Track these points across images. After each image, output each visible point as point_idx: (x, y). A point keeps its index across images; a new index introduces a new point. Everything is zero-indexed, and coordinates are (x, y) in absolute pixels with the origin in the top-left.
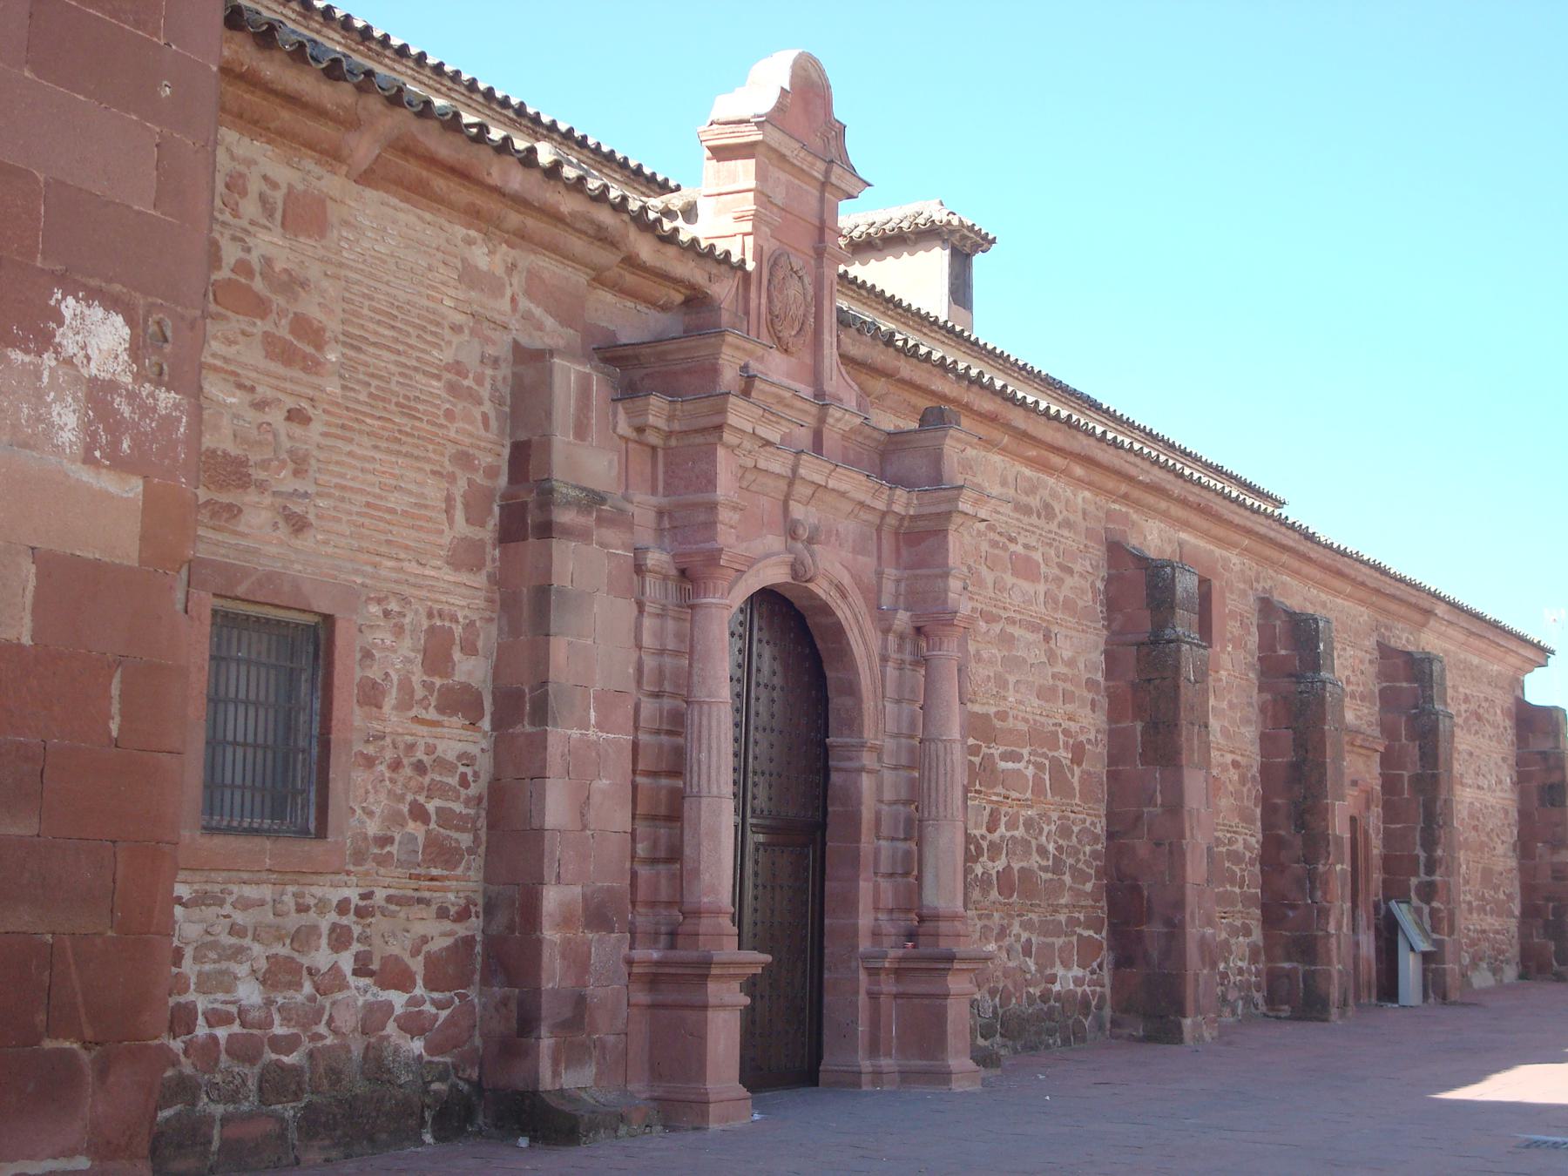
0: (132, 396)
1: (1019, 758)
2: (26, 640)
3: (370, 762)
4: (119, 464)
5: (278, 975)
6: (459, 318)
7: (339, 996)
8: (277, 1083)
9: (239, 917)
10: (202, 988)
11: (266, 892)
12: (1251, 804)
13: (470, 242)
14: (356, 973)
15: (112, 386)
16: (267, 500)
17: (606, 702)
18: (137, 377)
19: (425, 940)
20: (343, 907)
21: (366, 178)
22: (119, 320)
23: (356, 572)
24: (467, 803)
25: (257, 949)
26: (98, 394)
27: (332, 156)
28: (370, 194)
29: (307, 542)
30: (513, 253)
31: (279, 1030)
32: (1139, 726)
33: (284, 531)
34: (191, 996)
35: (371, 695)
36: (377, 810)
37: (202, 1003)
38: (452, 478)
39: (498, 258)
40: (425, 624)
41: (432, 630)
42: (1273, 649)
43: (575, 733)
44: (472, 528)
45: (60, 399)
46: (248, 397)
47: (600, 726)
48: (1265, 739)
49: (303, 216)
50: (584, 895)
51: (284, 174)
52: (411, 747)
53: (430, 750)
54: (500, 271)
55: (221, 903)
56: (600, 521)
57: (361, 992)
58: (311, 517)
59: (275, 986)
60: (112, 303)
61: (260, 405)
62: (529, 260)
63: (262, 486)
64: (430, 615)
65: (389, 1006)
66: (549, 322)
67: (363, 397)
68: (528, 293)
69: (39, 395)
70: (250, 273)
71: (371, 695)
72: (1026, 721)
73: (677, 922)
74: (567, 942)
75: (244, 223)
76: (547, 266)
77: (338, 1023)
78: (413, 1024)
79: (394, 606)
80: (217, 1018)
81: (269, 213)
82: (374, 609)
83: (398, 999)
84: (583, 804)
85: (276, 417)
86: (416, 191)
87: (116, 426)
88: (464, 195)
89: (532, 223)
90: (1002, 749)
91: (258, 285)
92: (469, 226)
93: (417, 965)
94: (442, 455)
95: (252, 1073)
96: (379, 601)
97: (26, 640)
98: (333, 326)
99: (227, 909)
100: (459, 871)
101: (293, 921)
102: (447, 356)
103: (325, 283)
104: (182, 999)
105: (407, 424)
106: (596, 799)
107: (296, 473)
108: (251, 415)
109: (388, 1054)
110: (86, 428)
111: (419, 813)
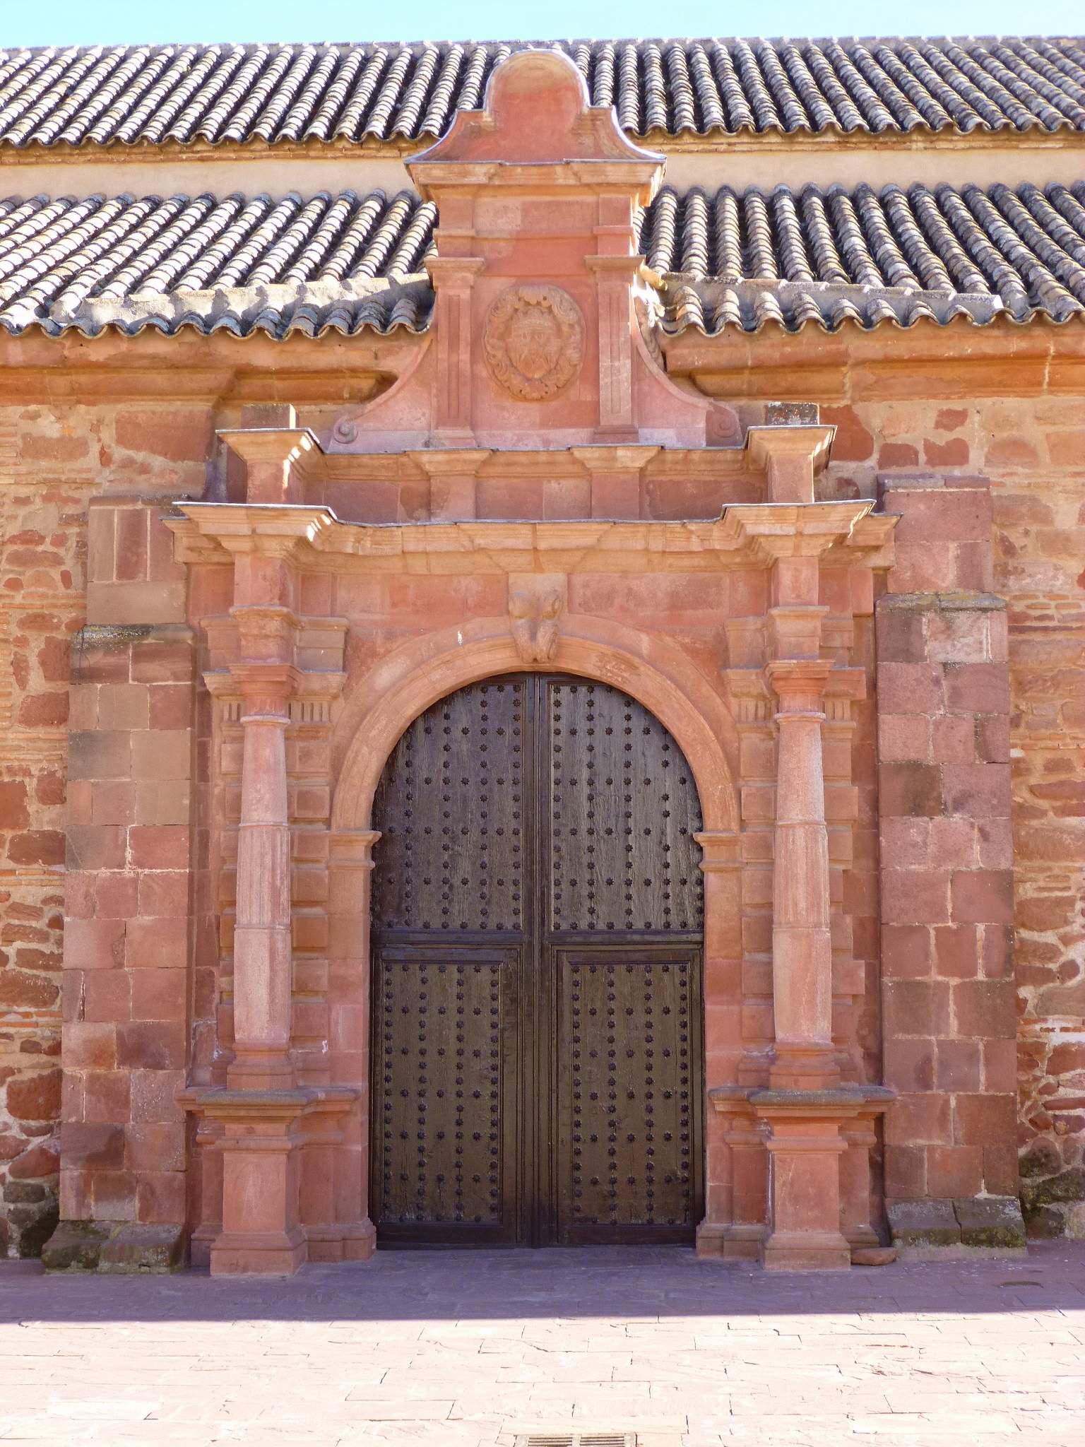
6: (24, 491)
13: (34, 417)
17: (147, 841)
30: (94, 410)
38: (22, 642)
39: (72, 421)
43: (104, 872)
44: (53, 684)
47: (139, 863)
50: (120, 1034)
56: (138, 657)
62: (110, 411)
66: (158, 462)
68: (121, 441)
74: (93, 1079)
76: (143, 408)
84: (115, 942)
92: (26, 403)
94: (8, 623)
100: (55, 1008)
106: (135, 935)
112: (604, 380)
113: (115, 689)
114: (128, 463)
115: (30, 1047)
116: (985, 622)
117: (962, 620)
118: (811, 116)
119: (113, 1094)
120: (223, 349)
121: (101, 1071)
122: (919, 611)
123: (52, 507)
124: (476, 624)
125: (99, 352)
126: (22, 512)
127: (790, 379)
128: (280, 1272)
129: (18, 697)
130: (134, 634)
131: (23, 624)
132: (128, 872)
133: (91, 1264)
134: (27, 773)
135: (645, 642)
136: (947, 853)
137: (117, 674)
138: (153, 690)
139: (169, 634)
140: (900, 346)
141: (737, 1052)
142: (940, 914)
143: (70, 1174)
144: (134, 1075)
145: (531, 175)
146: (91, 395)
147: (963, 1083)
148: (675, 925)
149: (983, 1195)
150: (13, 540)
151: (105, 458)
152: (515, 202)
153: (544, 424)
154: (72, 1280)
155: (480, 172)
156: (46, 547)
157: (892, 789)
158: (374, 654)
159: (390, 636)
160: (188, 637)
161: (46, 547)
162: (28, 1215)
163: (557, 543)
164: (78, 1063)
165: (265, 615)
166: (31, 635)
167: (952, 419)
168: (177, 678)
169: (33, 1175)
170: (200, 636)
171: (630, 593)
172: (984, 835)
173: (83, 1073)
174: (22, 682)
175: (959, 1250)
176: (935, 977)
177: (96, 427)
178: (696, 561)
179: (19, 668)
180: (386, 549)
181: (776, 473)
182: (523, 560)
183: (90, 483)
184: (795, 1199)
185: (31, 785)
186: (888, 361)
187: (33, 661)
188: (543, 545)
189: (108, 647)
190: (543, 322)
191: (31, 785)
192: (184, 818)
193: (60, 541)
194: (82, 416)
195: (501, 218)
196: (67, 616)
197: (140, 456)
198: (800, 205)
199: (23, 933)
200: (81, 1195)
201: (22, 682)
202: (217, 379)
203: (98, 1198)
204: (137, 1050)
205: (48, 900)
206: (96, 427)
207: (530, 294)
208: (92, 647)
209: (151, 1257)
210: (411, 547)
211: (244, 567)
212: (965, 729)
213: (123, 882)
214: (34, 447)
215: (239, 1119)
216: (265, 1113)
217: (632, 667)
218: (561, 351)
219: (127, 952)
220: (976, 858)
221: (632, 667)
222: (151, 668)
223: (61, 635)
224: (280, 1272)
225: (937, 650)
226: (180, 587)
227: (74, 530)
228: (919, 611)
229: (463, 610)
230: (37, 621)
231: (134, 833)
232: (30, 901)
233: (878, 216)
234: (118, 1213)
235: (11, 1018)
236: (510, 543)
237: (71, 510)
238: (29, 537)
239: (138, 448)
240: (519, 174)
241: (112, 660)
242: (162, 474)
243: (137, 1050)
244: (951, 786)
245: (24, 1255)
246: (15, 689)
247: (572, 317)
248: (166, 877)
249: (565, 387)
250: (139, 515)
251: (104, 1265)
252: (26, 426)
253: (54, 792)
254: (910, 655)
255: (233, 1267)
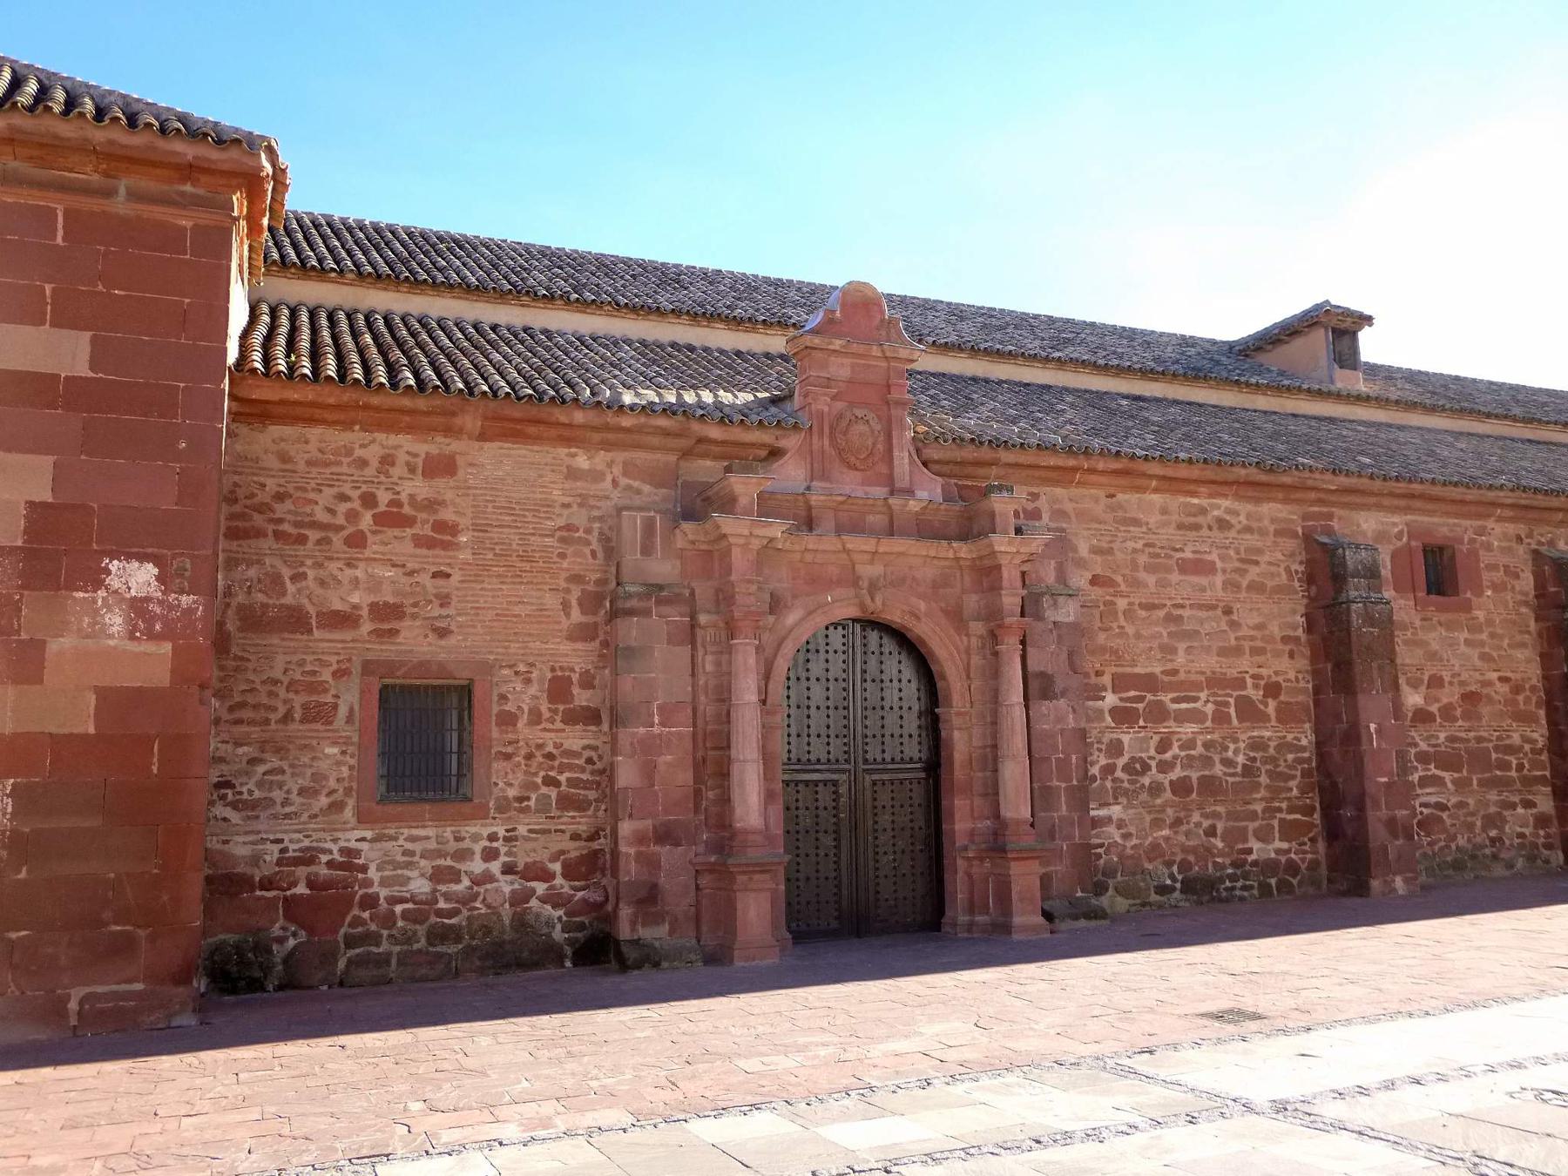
0: (160, 602)
1: (1196, 699)
2: (92, 730)
3: (508, 757)
4: (152, 636)
5: (438, 876)
6: (567, 500)
7: (488, 886)
8: (440, 935)
9: (409, 846)
10: (384, 882)
11: (430, 832)
12: (1533, 708)
13: (574, 455)
14: (503, 873)
15: (148, 599)
16: (418, 623)
18: (164, 593)
19: (563, 852)
20: (493, 837)
21: (483, 437)
22: (150, 566)
23: (491, 653)
24: (592, 773)
25: (423, 863)
26: (138, 607)
27: (449, 431)
28: (487, 445)
29: (452, 641)
31: (442, 905)
32: (1329, 666)
33: (432, 637)
34: (375, 889)
35: (508, 720)
36: (516, 783)
37: (383, 893)
38: (568, 591)
40: (549, 675)
41: (553, 680)
42: (1544, 587)
45: (110, 610)
46: (400, 571)
47: (662, 724)
48: (1545, 657)
49: (440, 467)
50: (654, 827)
51: (422, 448)
52: (540, 747)
53: (556, 746)
54: (601, 467)
55: (396, 839)
56: (659, 602)
57: (507, 885)
58: (453, 628)
59: (439, 882)
60: (142, 558)
61: (411, 573)
62: (620, 456)
63: (414, 617)
64: (553, 669)
65: (533, 891)
66: (646, 488)
67: (490, 556)
68: (625, 474)
69: (96, 611)
70: (399, 504)
71: (508, 720)
72: (1203, 673)
73: (724, 836)
74: (639, 854)
75: (395, 479)
76: (640, 456)
77: (489, 900)
78: (553, 899)
79: (522, 668)
80: (393, 901)
81: (412, 470)
82: (505, 672)
83: (540, 888)
84: (649, 771)
85: (425, 579)
86: (505, 435)
87: (150, 619)
88: (553, 432)
89: (611, 436)
90: (1171, 696)
91: (407, 510)
93: (557, 867)
95: (421, 930)
96: (510, 667)
97: (92, 730)
98: (464, 522)
99: (401, 842)
100: (590, 813)
101: (453, 846)
102: (561, 522)
103: (458, 500)
104: (370, 891)
105: (527, 566)
106: (662, 768)
107: (442, 605)
108: (404, 580)
109: (530, 918)
110: (128, 621)
111: (551, 782)
112: (896, 462)
113: (645, 621)
114: (629, 487)
115: (575, 837)
116: (1070, 601)
117: (1061, 599)
118: (282, 256)
119: (652, 863)
120: (696, 427)
121: (643, 849)
122: (1043, 594)
123: (584, 511)
124: (841, 592)
125: (626, 422)
126: (566, 512)
127: (969, 470)
128: (772, 960)
129: (565, 624)
130: (655, 590)
131: (568, 580)
132: (656, 730)
133: (656, 965)
134: (572, 670)
135: (922, 606)
136: (1059, 720)
137: (646, 613)
138: (668, 623)
139: (677, 590)
140: (1023, 458)
141: (969, 825)
142: (1056, 750)
143: (625, 912)
144: (664, 851)
145: (861, 349)
146: (607, 446)
147: (1070, 837)
148: (888, 759)
149: (1079, 894)
150: (560, 529)
151: (615, 483)
152: (847, 361)
153: (863, 484)
154: (634, 979)
155: (837, 344)
156: (580, 534)
157: (1034, 685)
158: (786, 606)
159: (795, 597)
160: (687, 593)
161: (580, 534)
162: (577, 940)
163: (887, 549)
164: (630, 844)
165: (750, 582)
166: (573, 587)
167: (1034, 497)
168: (682, 615)
169: (580, 914)
170: (693, 594)
171: (914, 579)
172: (1074, 711)
173: (632, 851)
174: (568, 615)
175: (1082, 923)
176: (1055, 783)
177: (610, 465)
178: (947, 563)
179: (566, 606)
180: (797, 547)
181: (998, 519)
182: (867, 557)
183: (607, 498)
184: (1021, 900)
185: (575, 677)
186: (1017, 465)
187: (574, 603)
188: (881, 550)
189: (640, 596)
190: (862, 427)
191: (575, 677)
192: (689, 699)
193: (588, 531)
194: (602, 458)
195: (841, 369)
196: (595, 576)
197: (636, 484)
198: (313, 315)
199: (570, 767)
200: (633, 924)
201: (568, 615)
202: (683, 443)
203: (643, 925)
204: (664, 835)
205: (584, 748)
206: (610, 465)
207: (859, 413)
208: (630, 596)
209: (693, 957)
210: (810, 547)
211: (736, 553)
212: (1064, 656)
213: (654, 736)
214: (573, 474)
215: (744, 873)
216: (762, 868)
217: (918, 618)
218: (874, 444)
219: (657, 778)
220: (1071, 722)
221: (918, 618)
222: (666, 610)
223: (591, 587)
224: (772, 960)
225: (1051, 615)
226: (678, 563)
227: (597, 525)
228: (1043, 594)
229: (830, 584)
230: (576, 579)
231: (660, 708)
232: (575, 748)
233: (344, 326)
234: (655, 934)
235: (565, 819)
236: (864, 548)
237: (596, 513)
238: (569, 527)
239: (635, 479)
240: (855, 348)
241: (642, 604)
242: (649, 495)
243: (664, 835)
244: (1059, 685)
245: (575, 965)
246: (563, 619)
247: (878, 427)
248: (679, 733)
249: (878, 464)
250: (652, 519)
251: (665, 964)
252: (568, 461)
253: (587, 682)
254: (1039, 617)
255: (747, 959)
